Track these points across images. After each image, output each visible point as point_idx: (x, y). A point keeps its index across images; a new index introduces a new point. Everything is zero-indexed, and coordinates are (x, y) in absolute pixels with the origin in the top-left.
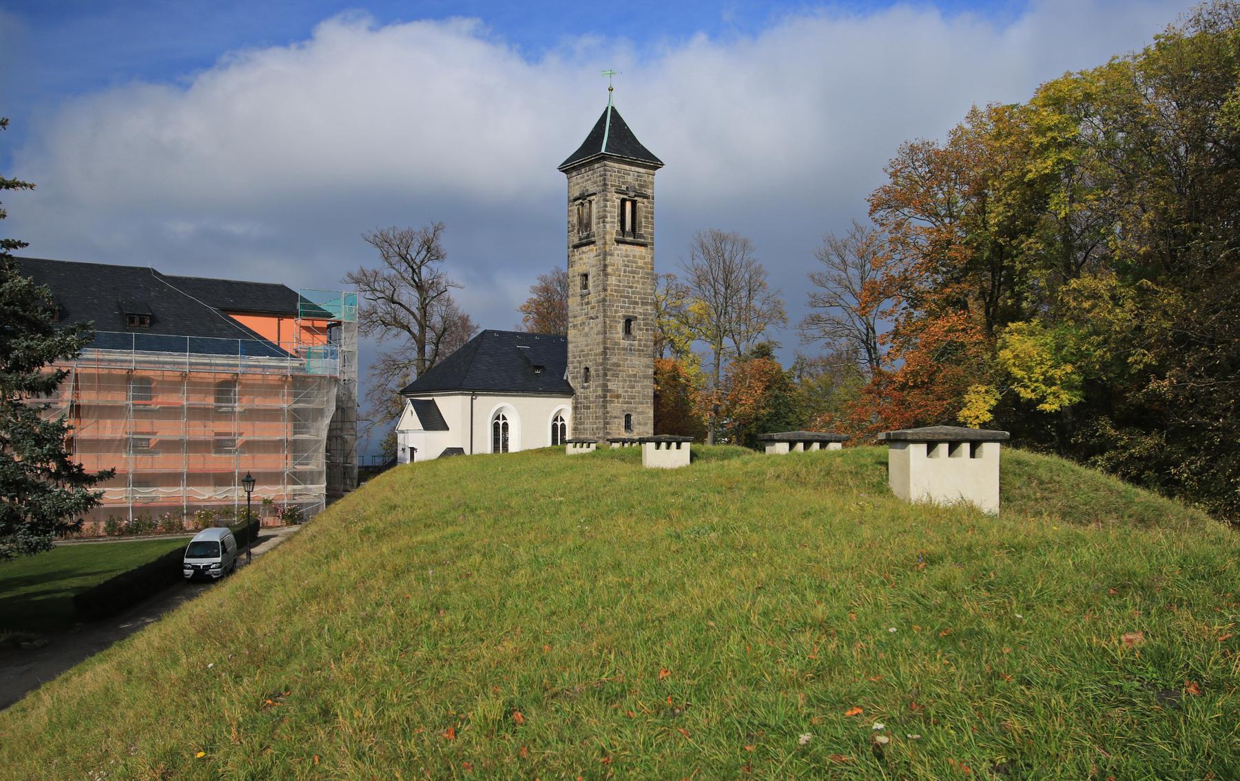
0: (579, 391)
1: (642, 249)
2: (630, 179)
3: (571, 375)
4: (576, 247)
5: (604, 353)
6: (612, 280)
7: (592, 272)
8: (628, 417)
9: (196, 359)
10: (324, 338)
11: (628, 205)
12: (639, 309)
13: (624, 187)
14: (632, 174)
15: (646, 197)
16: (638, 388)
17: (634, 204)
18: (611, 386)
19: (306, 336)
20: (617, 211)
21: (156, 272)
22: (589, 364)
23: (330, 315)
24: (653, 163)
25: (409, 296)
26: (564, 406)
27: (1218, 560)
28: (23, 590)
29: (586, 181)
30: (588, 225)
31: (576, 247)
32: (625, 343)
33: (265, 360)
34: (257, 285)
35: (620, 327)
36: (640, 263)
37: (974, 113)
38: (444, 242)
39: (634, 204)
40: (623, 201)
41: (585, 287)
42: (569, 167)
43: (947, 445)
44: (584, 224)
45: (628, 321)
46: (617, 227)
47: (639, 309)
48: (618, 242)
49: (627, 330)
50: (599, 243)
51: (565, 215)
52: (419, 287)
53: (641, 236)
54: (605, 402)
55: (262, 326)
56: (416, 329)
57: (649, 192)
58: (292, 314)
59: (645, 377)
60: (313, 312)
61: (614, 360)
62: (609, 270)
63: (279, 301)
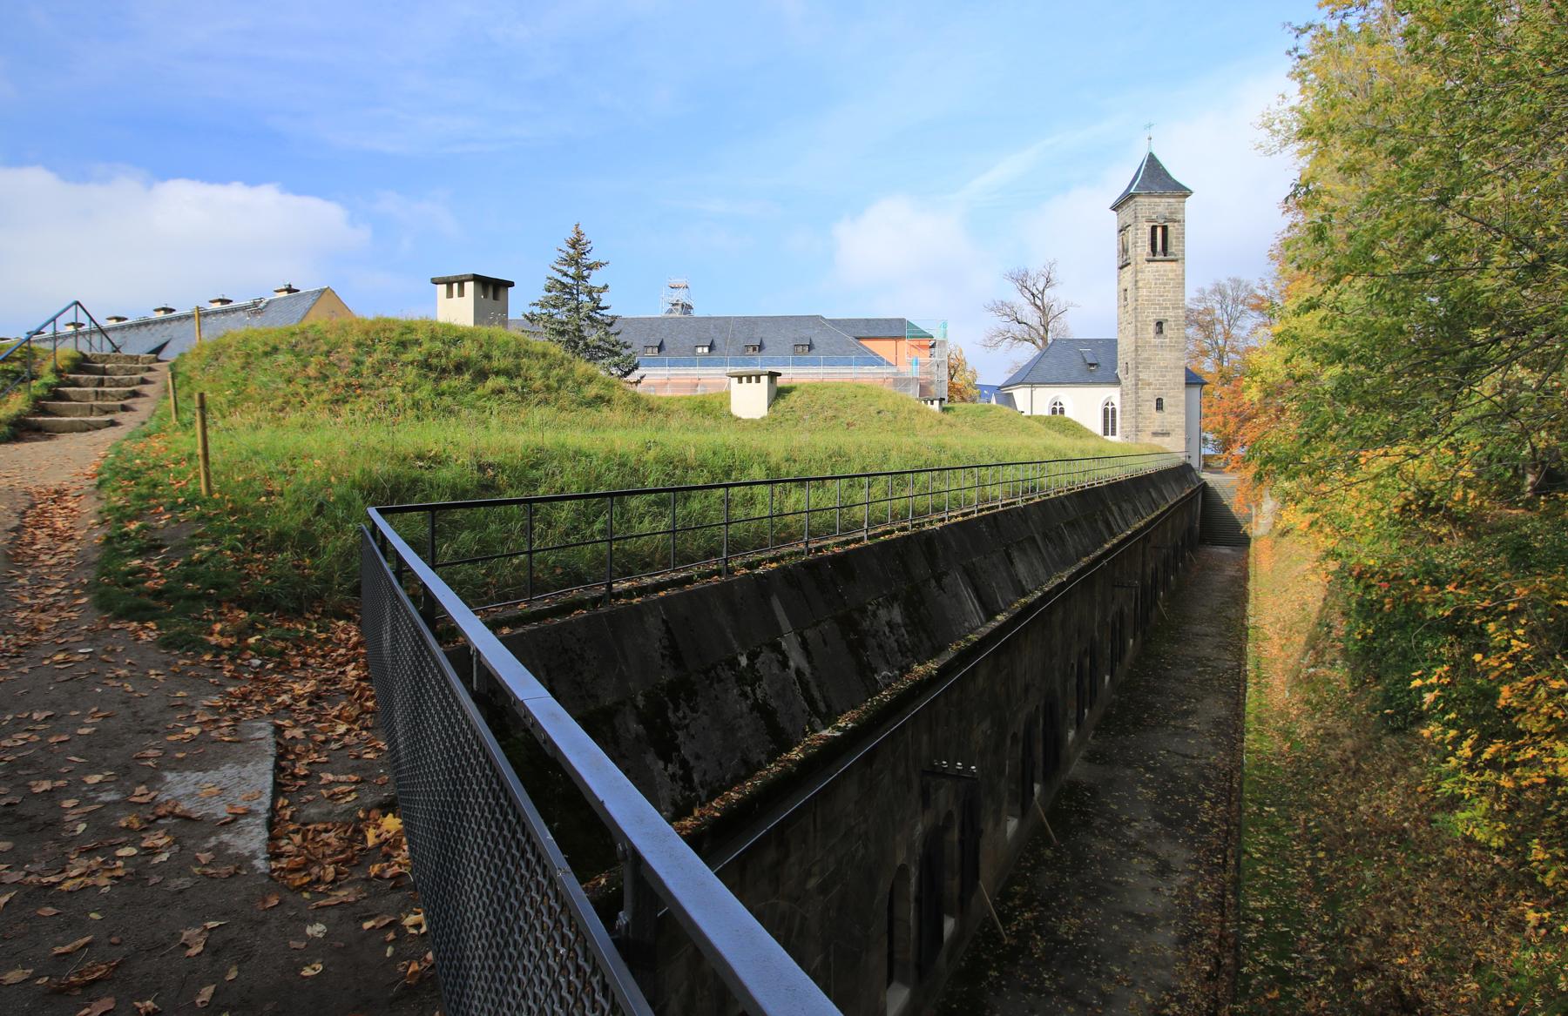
2: (1160, 209)
3: (1120, 372)
6: (1143, 292)
7: (1130, 286)
10: (928, 352)
11: (1159, 231)
12: (1170, 313)
14: (1160, 206)
15: (1175, 221)
17: (1165, 229)
18: (1142, 376)
20: (1148, 237)
24: (1182, 192)
25: (1032, 317)
26: (1113, 394)
27: (1250, 736)
28: (853, 546)
29: (1127, 212)
32: (1158, 341)
33: (874, 369)
35: (1152, 328)
36: (1171, 275)
39: (1165, 229)
40: (1154, 229)
42: (1116, 208)
44: (1125, 251)
45: (1159, 324)
46: (1148, 249)
52: (1043, 310)
55: (883, 348)
57: (1179, 217)
58: (902, 338)
60: (920, 335)
63: (896, 330)
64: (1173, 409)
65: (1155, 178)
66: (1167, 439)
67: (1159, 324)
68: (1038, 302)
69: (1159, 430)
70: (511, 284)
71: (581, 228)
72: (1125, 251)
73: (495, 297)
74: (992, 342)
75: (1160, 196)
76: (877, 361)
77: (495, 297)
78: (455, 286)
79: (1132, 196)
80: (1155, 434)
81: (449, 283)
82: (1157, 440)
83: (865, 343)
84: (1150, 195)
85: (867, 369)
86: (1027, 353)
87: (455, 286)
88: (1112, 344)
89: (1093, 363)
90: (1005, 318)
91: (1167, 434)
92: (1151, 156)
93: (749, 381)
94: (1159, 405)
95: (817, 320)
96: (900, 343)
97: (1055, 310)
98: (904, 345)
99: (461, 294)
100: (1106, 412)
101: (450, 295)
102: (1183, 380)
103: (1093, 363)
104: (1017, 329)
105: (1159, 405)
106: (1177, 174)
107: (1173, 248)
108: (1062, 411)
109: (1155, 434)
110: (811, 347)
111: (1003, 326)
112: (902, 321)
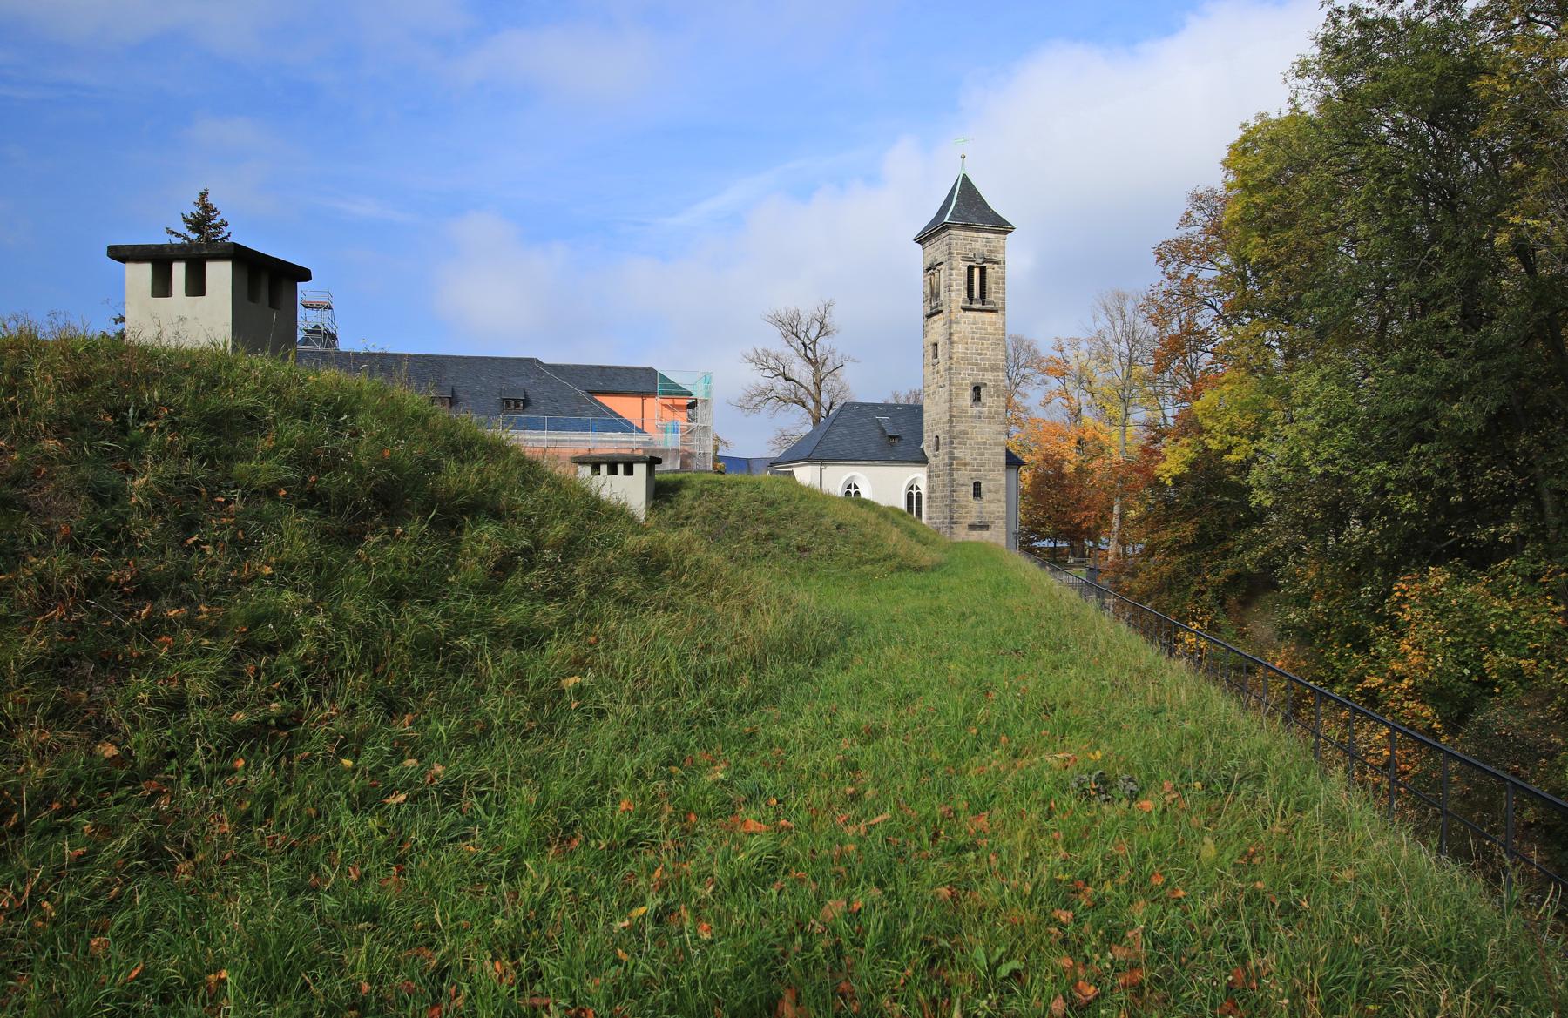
0: (932, 460)
1: (993, 315)
2: (977, 246)
3: (927, 447)
4: (929, 316)
5: (951, 421)
7: (941, 341)
8: (977, 486)
9: (555, 435)
10: (684, 415)
11: (976, 272)
12: (989, 376)
13: (971, 255)
14: (979, 242)
16: (988, 454)
17: (983, 270)
18: (957, 453)
19: (667, 413)
20: (964, 279)
21: (539, 362)
22: (939, 433)
23: (690, 394)
24: (1002, 227)
25: (802, 372)
26: (919, 475)
29: (937, 249)
30: (938, 295)
31: (929, 316)
32: (975, 410)
33: (618, 436)
34: (627, 369)
35: (968, 394)
36: (990, 329)
37: (1223, 163)
38: (833, 321)
40: (970, 269)
41: (936, 356)
42: (922, 239)
43: (644, 467)
44: (934, 294)
45: (977, 389)
46: (964, 294)
47: (989, 376)
48: (965, 309)
49: (977, 399)
50: (946, 311)
51: (917, 281)
52: (813, 363)
53: (991, 302)
54: (951, 469)
55: (625, 406)
56: (811, 404)
57: (999, 257)
58: (652, 394)
59: (996, 444)
60: (675, 391)
61: (961, 427)
62: (955, 338)
63: (643, 383)
64: (993, 496)
65: (968, 209)
66: (985, 534)
67: (977, 389)
68: (810, 354)
69: (976, 521)
70: (305, 275)
71: (210, 200)
72: (934, 294)
73: (274, 303)
74: (755, 401)
75: (978, 230)
76: (624, 426)
77: (274, 303)
78: (179, 270)
79: (947, 227)
80: (972, 527)
81: (160, 260)
82: (975, 536)
83: (607, 401)
84: (966, 227)
85: (608, 436)
86: (798, 423)
87: (179, 270)
88: (913, 413)
89: (892, 433)
90: (768, 373)
91: (985, 527)
92: (965, 178)
93: (613, 471)
94: (977, 492)
95: (531, 365)
96: (648, 401)
97: (829, 366)
98: (653, 404)
99: (196, 286)
100: (909, 497)
101: (162, 286)
102: (1003, 459)
103: (892, 433)
104: (780, 385)
105: (977, 492)
106: (997, 202)
107: (991, 296)
108: (857, 493)
109: (972, 527)
110: (527, 403)
111: (763, 383)
112: (650, 372)
